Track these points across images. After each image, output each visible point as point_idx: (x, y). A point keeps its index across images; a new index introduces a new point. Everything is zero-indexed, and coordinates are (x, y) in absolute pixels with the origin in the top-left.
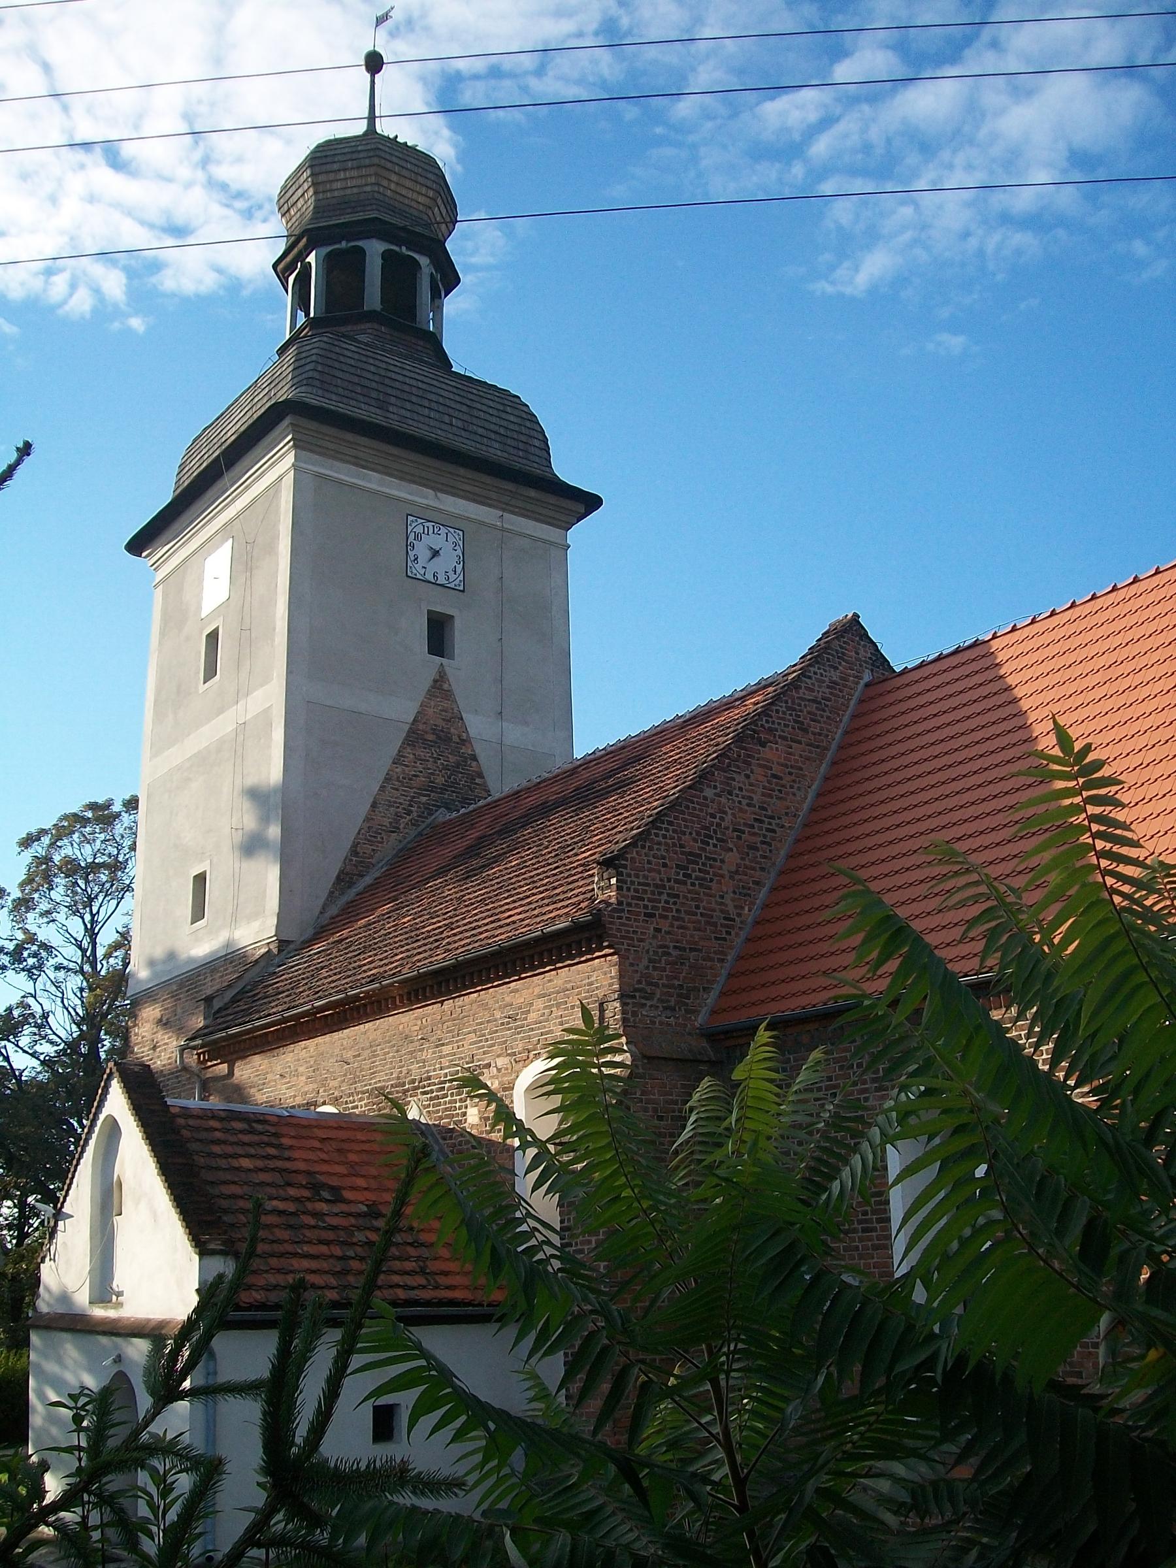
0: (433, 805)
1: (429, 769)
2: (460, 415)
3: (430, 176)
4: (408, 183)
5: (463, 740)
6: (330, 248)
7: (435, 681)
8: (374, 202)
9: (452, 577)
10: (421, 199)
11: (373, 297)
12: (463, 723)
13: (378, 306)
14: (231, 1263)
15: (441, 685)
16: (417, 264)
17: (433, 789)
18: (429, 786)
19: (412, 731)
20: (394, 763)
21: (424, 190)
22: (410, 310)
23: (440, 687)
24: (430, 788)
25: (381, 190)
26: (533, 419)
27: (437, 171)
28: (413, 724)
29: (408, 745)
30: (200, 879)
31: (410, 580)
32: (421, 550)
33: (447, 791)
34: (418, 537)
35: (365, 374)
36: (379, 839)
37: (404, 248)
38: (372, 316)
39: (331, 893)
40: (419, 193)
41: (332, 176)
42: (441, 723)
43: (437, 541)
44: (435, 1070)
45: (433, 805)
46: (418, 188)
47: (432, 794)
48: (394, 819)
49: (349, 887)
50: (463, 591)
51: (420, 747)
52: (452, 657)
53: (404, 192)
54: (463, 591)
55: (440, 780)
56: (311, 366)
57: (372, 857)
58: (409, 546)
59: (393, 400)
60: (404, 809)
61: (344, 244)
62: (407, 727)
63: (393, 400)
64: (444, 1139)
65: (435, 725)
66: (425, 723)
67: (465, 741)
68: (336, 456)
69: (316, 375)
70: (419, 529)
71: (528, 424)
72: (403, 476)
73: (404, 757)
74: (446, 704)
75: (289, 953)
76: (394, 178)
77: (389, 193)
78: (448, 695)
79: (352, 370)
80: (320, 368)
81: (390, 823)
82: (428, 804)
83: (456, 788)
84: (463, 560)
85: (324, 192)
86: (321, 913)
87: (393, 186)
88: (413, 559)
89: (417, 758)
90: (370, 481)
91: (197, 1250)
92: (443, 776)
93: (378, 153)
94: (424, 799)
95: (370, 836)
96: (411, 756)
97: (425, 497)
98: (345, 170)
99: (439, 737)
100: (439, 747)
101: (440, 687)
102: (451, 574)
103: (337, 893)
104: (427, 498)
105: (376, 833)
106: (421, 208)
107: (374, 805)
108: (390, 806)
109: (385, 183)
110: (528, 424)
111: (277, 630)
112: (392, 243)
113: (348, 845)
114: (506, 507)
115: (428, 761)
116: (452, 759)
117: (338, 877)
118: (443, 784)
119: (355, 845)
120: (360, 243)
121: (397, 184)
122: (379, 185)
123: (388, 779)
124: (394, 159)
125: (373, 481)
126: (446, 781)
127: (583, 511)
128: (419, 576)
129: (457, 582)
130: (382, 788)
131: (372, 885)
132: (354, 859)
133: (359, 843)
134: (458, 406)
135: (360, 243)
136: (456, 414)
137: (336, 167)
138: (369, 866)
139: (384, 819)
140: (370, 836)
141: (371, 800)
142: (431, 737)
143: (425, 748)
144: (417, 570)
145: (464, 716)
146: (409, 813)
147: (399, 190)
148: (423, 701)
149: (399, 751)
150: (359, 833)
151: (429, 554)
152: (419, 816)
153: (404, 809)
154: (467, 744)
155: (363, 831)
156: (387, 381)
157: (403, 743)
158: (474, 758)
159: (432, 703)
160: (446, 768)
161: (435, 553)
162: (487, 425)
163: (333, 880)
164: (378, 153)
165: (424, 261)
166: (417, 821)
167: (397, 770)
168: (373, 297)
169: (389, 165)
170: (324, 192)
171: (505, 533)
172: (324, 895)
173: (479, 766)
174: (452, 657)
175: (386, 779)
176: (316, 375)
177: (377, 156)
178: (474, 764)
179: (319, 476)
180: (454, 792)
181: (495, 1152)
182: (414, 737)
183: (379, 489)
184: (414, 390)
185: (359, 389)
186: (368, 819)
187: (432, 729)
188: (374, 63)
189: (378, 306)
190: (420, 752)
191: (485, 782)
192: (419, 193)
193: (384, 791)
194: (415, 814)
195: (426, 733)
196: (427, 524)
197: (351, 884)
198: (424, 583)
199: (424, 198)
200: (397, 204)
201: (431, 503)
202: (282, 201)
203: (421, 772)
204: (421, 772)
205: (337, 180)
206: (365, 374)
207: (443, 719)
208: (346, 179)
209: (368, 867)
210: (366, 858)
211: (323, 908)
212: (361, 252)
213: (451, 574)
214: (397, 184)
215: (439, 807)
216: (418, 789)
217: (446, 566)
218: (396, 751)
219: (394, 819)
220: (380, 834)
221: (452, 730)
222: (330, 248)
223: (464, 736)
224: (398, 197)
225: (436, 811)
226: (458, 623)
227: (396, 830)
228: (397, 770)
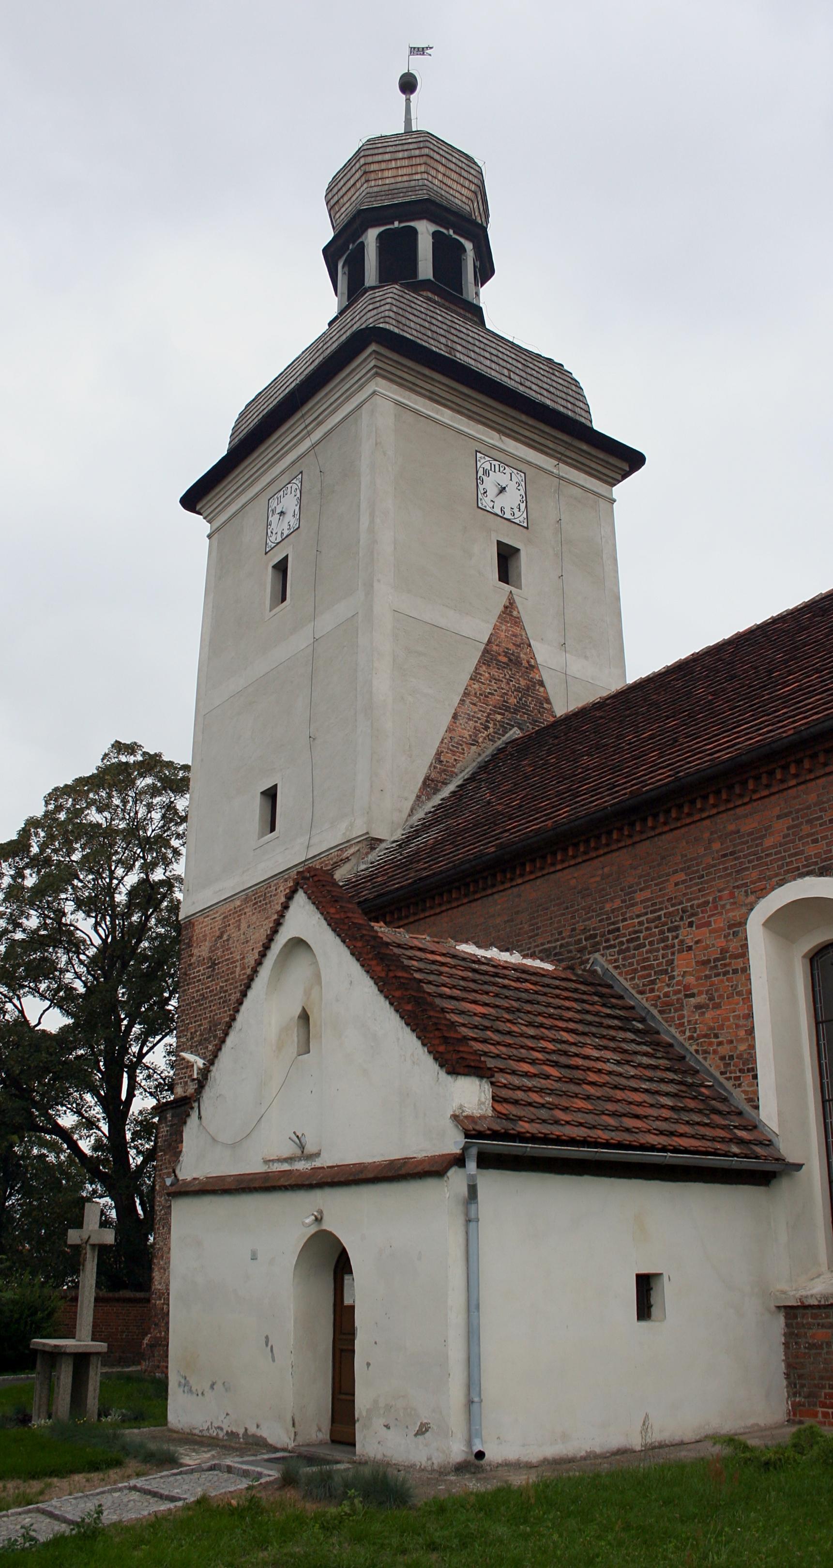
0: (507, 724)
1: (502, 689)
2: (517, 371)
3: (472, 171)
4: (454, 176)
5: (531, 666)
6: (382, 229)
7: (506, 607)
8: (425, 187)
9: (517, 514)
10: (465, 192)
11: (425, 269)
12: (532, 651)
13: (430, 276)
14: (486, 1087)
15: (511, 612)
16: (463, 249)
17: (507, 709)
18: (503, 705)
19: (486, 651)
20: (471, 679)
21: (467, 183)
22: (458, 286)
23: (510, 609)
24: (504, 707)
25: (430, 178)
26: (576, 383)
27: (477, 168)
28: (487, 645)
29: (484, 664)
30: (271, 795)
31: (480, 510)
32: (490, 484)
33: (519, 711)
34: (486, 473)
35: (434, 321)
36: (460, 750)
37: (451, 232)
38: (425, 285)
39: (418, 797)
40: (463, 186)
41: (383, 166)
42: (511, 646)
43: (504, 480)
44: (624, 920)
45: (507, 724)
46: (462, 180)
47: (507, 713)
48: (474, 733)
49: (434, 794)
50: (527, 528)
51: (494, 667)
52: (519, 587)
53: (449, 182)
54: (527, 528)
55: (513, 701)
56: (387, 307)
57: (454, 766)
58: (478, 480)
59: (459, 348)
60: (481, 724)
61: (396, 224)
62: (483, 647)
63: (459, 348)
64: (641, 993)
65: (507, 649)
66: (497, 645)
67: (533, 667)
68: (412, 388)
69: (392, 314)
70: (487, 466)
71: (574, 388)
72: (471, 416)
73: (481, 674)
74: (517, 630)
75: (381, 851)
76: (441, 169)
77: (436, 182)
78: (517, 622)
79: (423, 316)
80: (395, 309)
81: (470, 736)
82: (503, 722)
83: (527, 710)
84: (526, 498)
85: (375, 180)
86: (409, 815)
87: (440, 177)
88: (483, 492)
89: (492, 678)
90: (442, 415)
91: (444, 1070)
92: (515, 697)
93: (428, 144)
94: (499, 717)
95: (453, 746)
96: (487, 675)
97: (492, 438)
98: (396, 160)
99: (510, 660)
100: (511, 670)
101: (510, 609)
102: (516, 510)
103: (424, 798)
104: (493, 439)
105: (457, 743)
106: (464, 199)
107: (455, 716)
108: (469, 719)
109: (433, 172)
110: (574, 388)
111: (361, 543)
112: (441, 226)
113: (433, 752)
114: (561, 458)
115: (502, 681)
116: (523, 682)
117: (424, 783)
118: (515, 705)
119: (439, 754)
120: (412, 224)
121: (444, 175)
122: (428, 174)
123: (466, 694)
124: (441, 152)
125: (446, 416)
126: (517, 702)
127: (627, 469)
128: (488, 509)
129: (521, 519)
130: (462, 701)
131: (439, 805)
132: (438, 766)
133: (442, 752)
134: (514, 363)
135: (412, 224)
136: (513, 369)
137: (387, 157)
138: (453, 775)
139: (465, 731)
140: (453, 746)
141: (453, 711)
142: (505, 660)
143: (499, 669)
144: (486, 503)
145: (532, 643)
146: (486, 728)
147: (446, 180)
148: (495, 625)
149: (476, 669)
150: (442, 742)
151: (496, 491)
152: (495, 733)
153: (481, 724)
154: (535, 670)
155: (446, 741)
156: (453, 331)
157: (479, 661)
158: (541, 683)
159: (504, 627)
160: (518, 690)
161: (503, 490)
162: (540, 383)
163: (420, 784)
164: (428, 144)
165: (468, 246)
166: (494, 737)
167: (475, 686)
168: (425, 269)
169: (437, 157)
170: (375, 180)
171: (561, 481)
172: (413, 797)
173: (546, 692)
174: (519, 587)
175: (465, 693)
176: (392, 314)
177: (427, 147)
178: (542, 689)
179: (398, 403)
180: (524, 713)
181: (721, 996)
182: (488, 657)
183: (451, 423)
184: (477, 343)
185: (429, 333)
186: (449, 730)
187: (504, 652)
188: (408, 85)
189: (430, 276)
190: (494, 672)
191: (552, 708)
192: (463, 186)
193: (463, 705)
194: (491, 730)
195: (499, 654)
196: (494, 462)
197: (436, 791)
198: (492, 515)
199: (466, 190)
200: (443, 193)
201: (497, 444)
202: (330, 196)
203: (496, 691)
204: (496, 691)
205: (388, 169)
206: (434, 321)
207: (514, 644)
208: (397, 168)
209: (452, 776)
210: (448, 767)
211: (412, 811)
212: (414, 232)
213: (516, 510)
214: (444, 175)
215: (513, 726)
216: (495, 707)
217: (511, 501)
218: (473, 669)
219: (474, 733)
220: (461, 745)
221: (522, 655)
222: (382, 229)
223: (532, 662)
224: (444, 187)
225: (510, 729)
226: (523, 554)
227: (475, 742)
228: (475, 686)
